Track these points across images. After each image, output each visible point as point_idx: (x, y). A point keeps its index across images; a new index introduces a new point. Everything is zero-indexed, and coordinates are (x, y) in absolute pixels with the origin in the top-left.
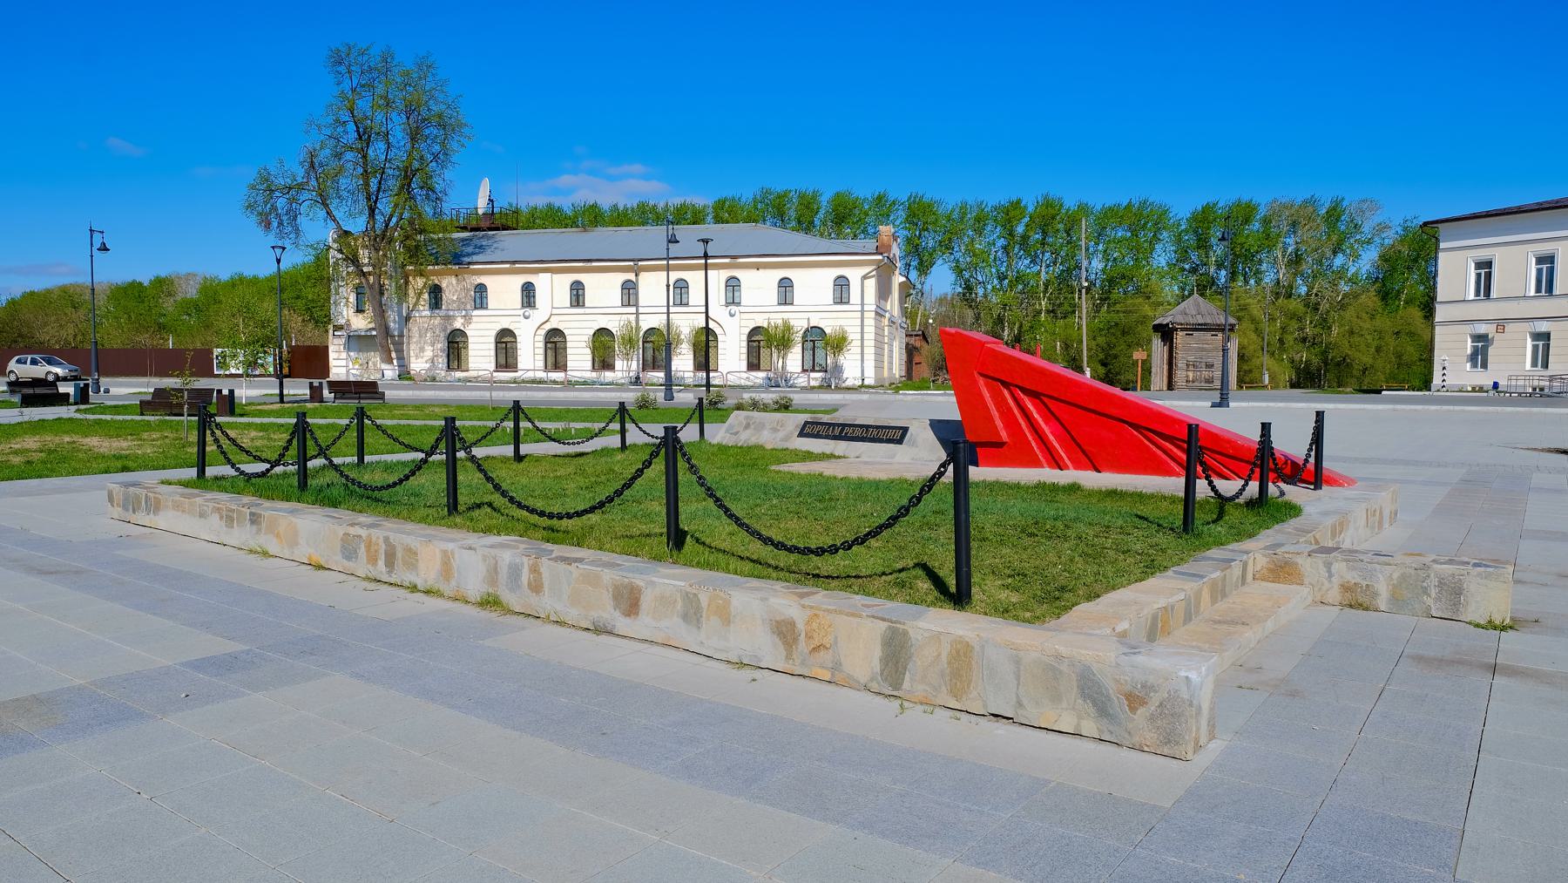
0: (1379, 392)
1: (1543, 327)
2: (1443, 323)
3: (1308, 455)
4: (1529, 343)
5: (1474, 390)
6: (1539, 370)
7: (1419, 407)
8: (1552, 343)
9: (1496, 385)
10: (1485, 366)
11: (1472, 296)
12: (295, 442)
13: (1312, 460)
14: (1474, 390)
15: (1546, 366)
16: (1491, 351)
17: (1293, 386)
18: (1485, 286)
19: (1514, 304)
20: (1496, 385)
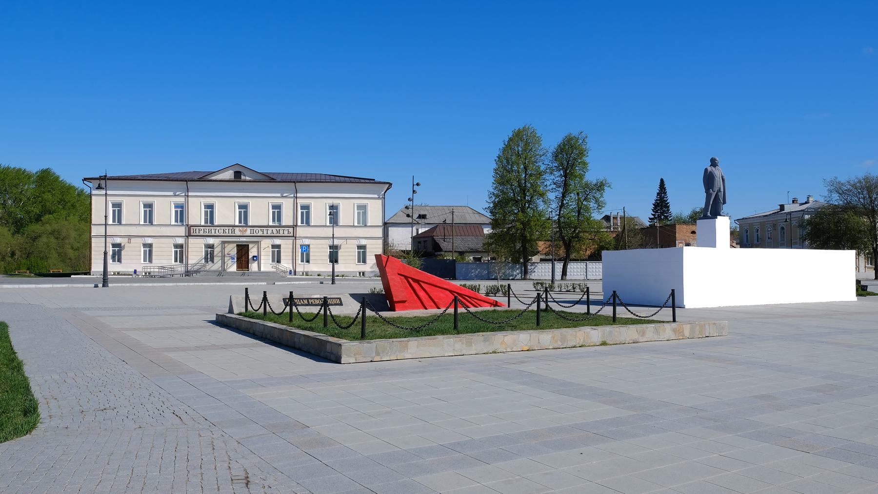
0: (69, 275)
1: (149, 241)
2: (96, 236)
3: (358, 314)
4: (142, 249)
5: (114, 274)
6: (147, 263)
7: (82, 285)
8: (154, 249)
9: (135, 271)
10: (119, 260)
11: (142, 223)
12: (635, 317)
13: (360, 315)
14: (114, 274)
15: (150, 261)
16: (123, 253)
17: (858, 282)
18: (149, 219)
19: (134, 228)
20: (135, 271)
